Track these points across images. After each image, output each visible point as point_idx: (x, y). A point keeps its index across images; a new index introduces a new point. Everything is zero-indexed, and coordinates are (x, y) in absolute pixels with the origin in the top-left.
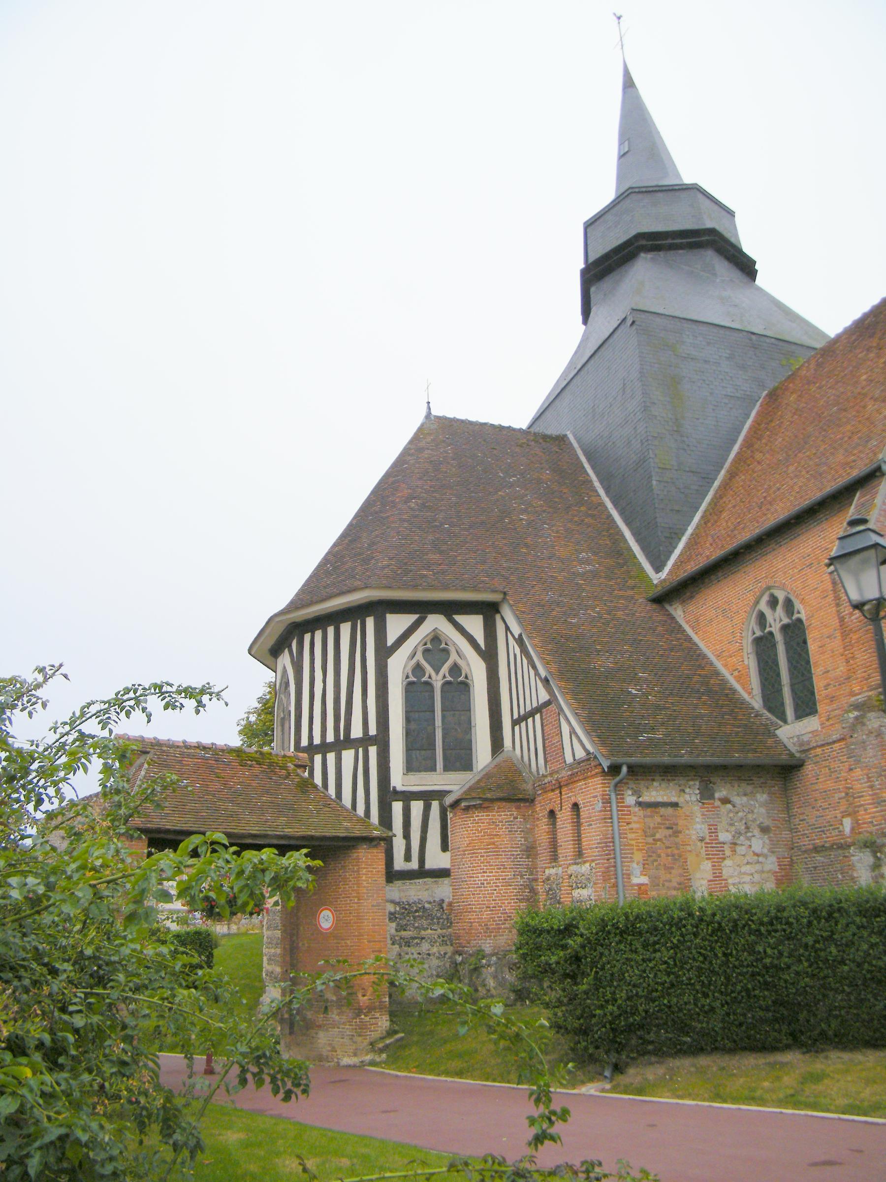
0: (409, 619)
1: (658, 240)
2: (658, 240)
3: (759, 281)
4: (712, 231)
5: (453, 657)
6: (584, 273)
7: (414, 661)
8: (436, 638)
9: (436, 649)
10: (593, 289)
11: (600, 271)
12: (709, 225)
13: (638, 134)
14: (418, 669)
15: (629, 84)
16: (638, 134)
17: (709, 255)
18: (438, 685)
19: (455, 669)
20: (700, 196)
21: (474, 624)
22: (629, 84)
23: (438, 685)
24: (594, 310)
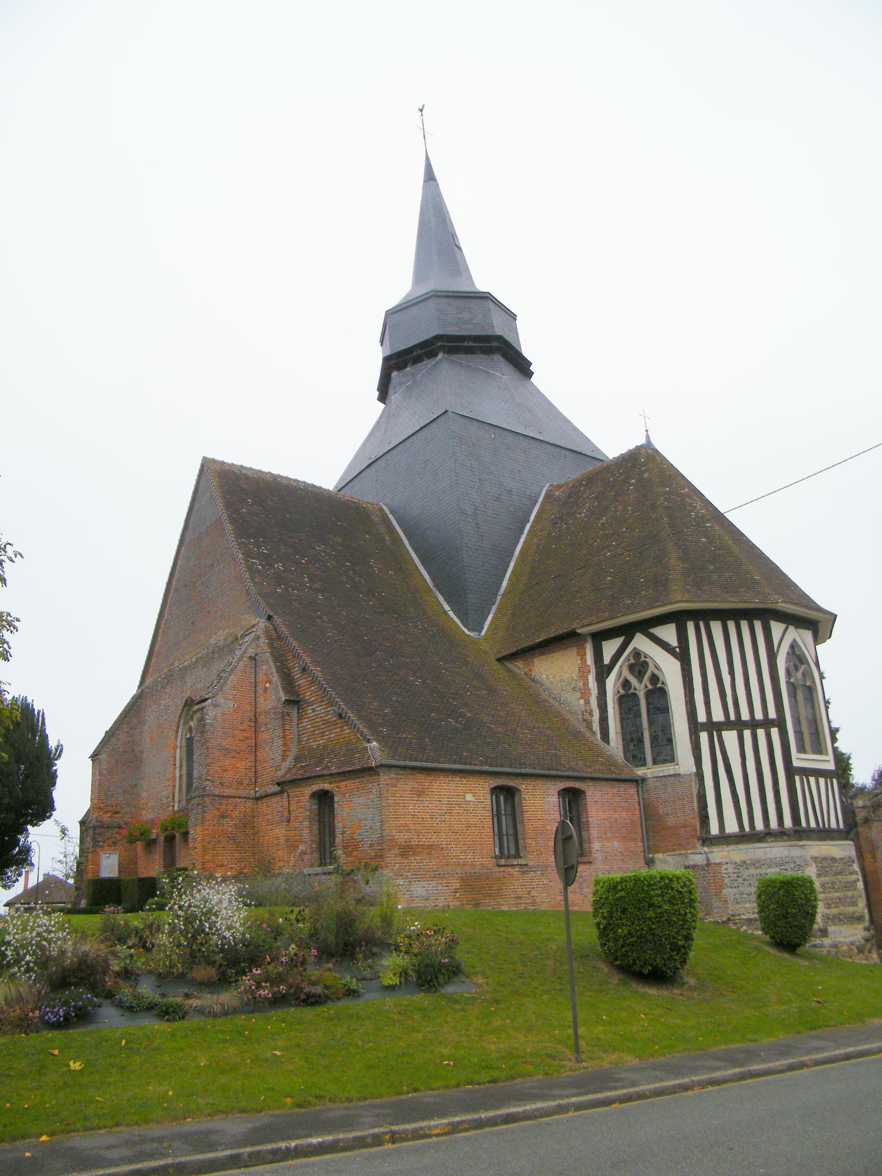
0: (617, 642)
1: (449, 341)
2: (449, 341)
3: (533, 379)
4: (500, 338)
5: (651, 668)
6: (387, 360)
7: (622, 679)
8: (637, 654)
9: (639, 665)
10: (394, 374)
11: (397, 363)
12: (498, 332)
13: (437, 236)
14: (626, 684)
15: (430, 176)
16: (437, 236)
17: (498, 357)
18: (641, 695)
19: (654, 679)
20: (491, 304)
21: (668, 633)
22: (430, 176)
23: (641, 695)
24: (391, 391)
